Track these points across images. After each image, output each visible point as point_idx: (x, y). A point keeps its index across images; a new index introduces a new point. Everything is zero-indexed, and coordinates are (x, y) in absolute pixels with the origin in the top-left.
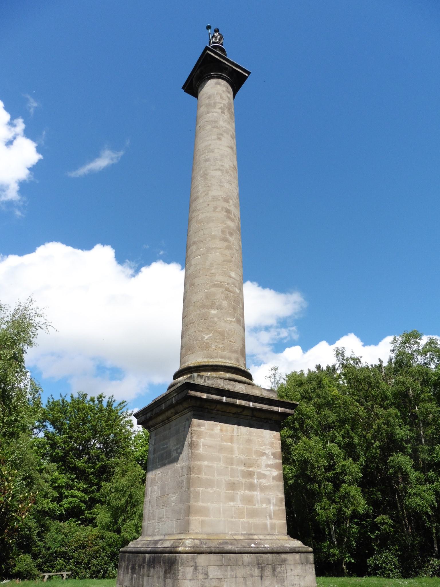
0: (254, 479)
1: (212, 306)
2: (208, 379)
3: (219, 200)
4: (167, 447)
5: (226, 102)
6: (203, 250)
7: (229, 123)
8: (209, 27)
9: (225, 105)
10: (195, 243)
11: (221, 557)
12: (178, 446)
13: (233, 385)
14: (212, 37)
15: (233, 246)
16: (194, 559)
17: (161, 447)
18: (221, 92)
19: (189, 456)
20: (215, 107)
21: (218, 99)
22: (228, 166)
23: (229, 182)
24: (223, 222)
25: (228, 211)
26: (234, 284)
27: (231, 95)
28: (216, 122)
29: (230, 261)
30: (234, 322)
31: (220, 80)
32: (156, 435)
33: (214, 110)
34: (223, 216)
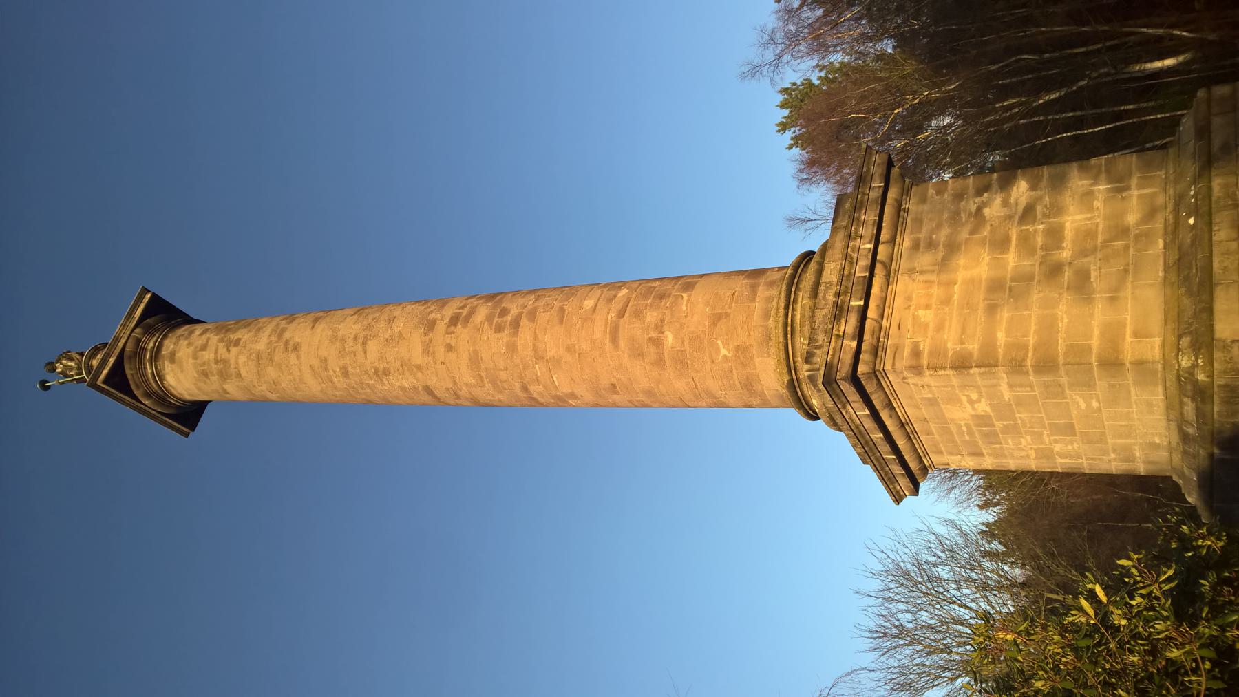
0: (1036, 231)
1: (657, 343)
2: (816, 341)
3: (431, 341)
4: (968, 426)
5: (214, 339)
6: (539, 369)
7: (259, 329)
8: (44, 386)
9: (221, 340)
10: (525, 388)
11: (1219, 288)
12: (964, 399)
13: (827, 288)
14: (66, 376)
15: (529, 307)
16: (1226, 347)
17: (967, 438)
18: (191, 350)
19: (984, 373)
20: (225, 362)
21: (208, 355)
22: (356, 327)
23: (391, 320)
24: (479, 329)
25: (454, 321)
26: (610, 301)
27: (199, 329)
28: (259, 356)
29: (562, 310)
30: (689, 296)
31: (164, 352)
32: (941, 453)
33: (232, 361)
34: (465, 331)
